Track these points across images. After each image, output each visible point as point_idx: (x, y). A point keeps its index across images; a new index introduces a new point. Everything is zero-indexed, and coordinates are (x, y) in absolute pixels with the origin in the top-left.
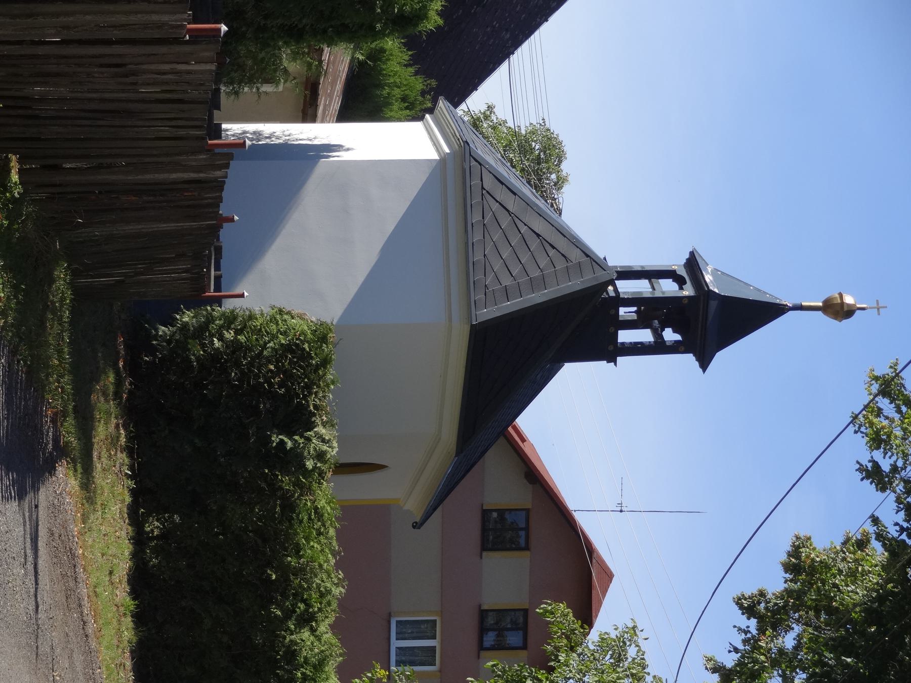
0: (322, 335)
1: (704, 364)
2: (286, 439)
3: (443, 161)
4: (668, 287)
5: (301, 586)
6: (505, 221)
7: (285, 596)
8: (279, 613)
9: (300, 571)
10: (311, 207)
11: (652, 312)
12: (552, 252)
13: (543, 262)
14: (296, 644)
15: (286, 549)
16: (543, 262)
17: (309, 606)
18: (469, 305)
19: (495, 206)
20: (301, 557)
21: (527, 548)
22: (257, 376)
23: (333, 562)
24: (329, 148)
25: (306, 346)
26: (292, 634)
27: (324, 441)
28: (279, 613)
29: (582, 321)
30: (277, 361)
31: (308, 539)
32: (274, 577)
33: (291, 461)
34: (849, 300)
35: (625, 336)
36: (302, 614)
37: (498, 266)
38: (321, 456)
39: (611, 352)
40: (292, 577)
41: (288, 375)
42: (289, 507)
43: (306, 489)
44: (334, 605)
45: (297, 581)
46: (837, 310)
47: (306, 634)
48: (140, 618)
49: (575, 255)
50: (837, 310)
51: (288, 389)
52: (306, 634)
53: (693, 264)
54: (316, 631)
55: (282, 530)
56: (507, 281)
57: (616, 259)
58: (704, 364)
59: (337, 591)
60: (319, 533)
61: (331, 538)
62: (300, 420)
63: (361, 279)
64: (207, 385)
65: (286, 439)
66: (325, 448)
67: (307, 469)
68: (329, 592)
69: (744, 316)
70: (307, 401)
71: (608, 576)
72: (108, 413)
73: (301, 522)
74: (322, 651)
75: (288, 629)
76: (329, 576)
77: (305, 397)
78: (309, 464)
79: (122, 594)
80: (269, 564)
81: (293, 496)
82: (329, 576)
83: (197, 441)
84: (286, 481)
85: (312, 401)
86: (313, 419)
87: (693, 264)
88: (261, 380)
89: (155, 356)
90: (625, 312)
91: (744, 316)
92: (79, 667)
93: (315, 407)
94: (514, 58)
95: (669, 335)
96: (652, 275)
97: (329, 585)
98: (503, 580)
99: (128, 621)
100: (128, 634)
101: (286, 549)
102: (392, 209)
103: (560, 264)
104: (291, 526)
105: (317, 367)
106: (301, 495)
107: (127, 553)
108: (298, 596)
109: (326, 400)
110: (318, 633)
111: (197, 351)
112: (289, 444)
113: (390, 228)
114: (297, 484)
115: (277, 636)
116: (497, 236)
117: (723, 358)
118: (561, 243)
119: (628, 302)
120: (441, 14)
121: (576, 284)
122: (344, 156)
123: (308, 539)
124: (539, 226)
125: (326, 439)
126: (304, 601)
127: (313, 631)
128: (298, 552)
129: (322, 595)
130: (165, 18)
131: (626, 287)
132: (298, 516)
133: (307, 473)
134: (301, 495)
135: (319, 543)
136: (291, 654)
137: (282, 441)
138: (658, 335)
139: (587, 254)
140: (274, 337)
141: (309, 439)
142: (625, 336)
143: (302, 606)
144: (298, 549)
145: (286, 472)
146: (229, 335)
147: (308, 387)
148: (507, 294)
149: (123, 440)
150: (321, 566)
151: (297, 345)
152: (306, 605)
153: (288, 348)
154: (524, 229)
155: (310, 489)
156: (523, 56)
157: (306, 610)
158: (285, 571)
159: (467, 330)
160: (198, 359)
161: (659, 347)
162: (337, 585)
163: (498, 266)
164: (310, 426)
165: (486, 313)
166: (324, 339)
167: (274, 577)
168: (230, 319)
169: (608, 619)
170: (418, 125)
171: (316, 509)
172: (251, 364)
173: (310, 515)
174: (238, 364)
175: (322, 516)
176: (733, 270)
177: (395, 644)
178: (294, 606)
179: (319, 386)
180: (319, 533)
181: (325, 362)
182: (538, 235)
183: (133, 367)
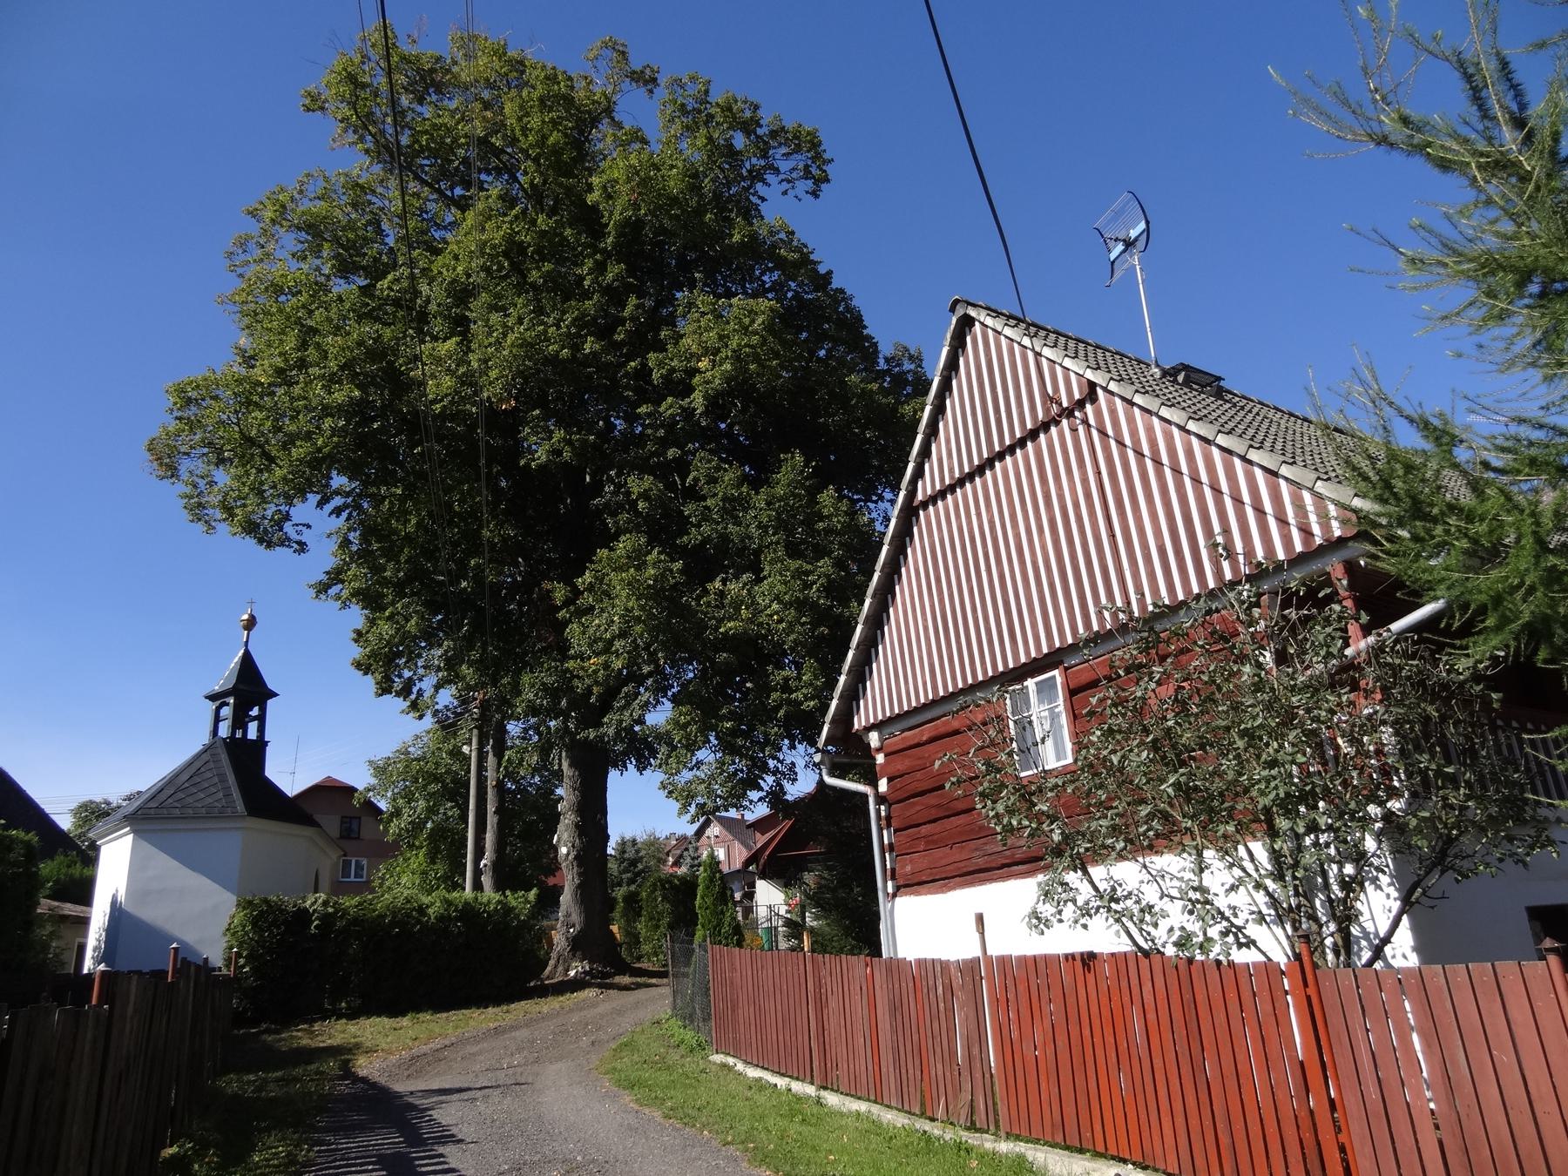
0: (245, 904)
3: (134, 831)
4: (226, 712)
9: (394, 914)
10: (151, 914)
11: (240, 721)
13: (209, 775)
16: (209, 775)
18: (235, 817)
24: (114, 903)
29: (245, 756)
33: (327, 920)
34: (246, 617)
37: (210, 800)
38: (325, 904)
42: (356, 921)
43: (345, 912)
46: (251, 624)
47: (431, 911)
48: (418, 1009)
49: (206, 757)
50: (251, 624)
52: (431, 911)
53: (212, 697)
56: (221, 795)
57: (204, 738)
62: (303, 915)
69: (248, 668)
72: (292, 1037)
79: (405, 1021)
85: (290, 908)
87: (212, 697)
90: (239, 734)
91: (248, 668)
92: (475, 1049)
94: (47, 811)
95: (255, 712)
96: (217, 719)
99: (421, 1015)
100: (427, 1016)
102: (164, 864)
103: (212, 765)
108: (408, 915)
109: (289, 901)
114: (342, 917)
116: (190, 800)
118: (198, 764)
119: (233, 733)
120: (27, 832)
121: (224, 757)
122: (122, 896)
124: (185, 777)
125: (314, 901)
130: (89, 1036)
131: (224, 731)
138: (255, 718)
139: (204, 751)
140: (247, 934)
142: (252, 733)
147: (281, 911)
148: (228, 795)
153: (254, 924)
156: (48, 808)
158: (393, 924)
161: (261, 719)
163: (210, 800)
164: (306, 910)
165: (240, 807)
166: (250, 903)
168: (228, 961)
169: (359, 778)
170: (103, 849)
172: (263, 947)
176: (224, 674)
177: (352, 879)
181: (266, 901)
183: (256, 1023)
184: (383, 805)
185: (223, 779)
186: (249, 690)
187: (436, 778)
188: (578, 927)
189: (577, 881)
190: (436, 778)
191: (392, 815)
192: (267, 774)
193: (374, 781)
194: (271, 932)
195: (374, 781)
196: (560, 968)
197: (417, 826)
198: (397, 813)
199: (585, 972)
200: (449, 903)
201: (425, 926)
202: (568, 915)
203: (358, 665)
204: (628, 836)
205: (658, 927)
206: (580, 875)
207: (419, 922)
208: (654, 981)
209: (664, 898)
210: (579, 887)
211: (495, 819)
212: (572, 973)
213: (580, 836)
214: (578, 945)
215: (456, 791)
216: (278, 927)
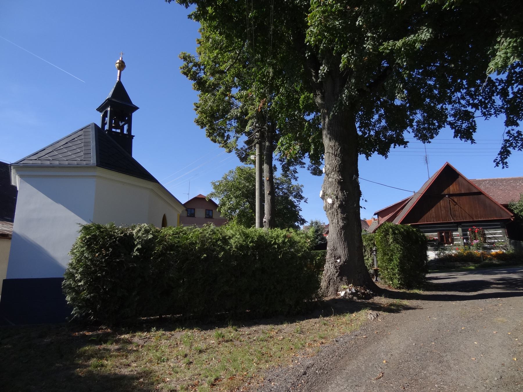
1: (136, 108)
2: (136, 248)
5: (209, 243)
6: (56, 153)
7: (214, 250)
8: (222, 253)
9: (203, 243)
12: (76, 139)
14: (237, 245)
15: (192, 250)
17: (219, 239)
19: (47, 156)
20: (196, 242)
21: (194, 209)
22: (101, 262)
23: (198, 229)
25: (87, 237)
26: (232, 247)
27: (140, 230)
28: (222, 253)
30: (94, 252)
31: (187, 239)
32: (205, 255)
33: (148, 246)
35: (125, 132)
36: (223, 242)
39: (130, 137)
40: (205, 247)
41: (103, 246)
42: (172, 247)
43: (163, 239)
44: (218, 228)
45: (208, 244)
47: (232, 241)
50: (122, 66)
51: (110, 246)
52: (232, 241)
54: (230, 237)
55: (183, 251)
58: (136, 108)
59: (212, 227)
60: (185, 234)
61: (187, 228)
62: (127, 241)
63: (72, 214)
64: (104, 289)
65: (136, 248)
66: (143, 230)
67: (152, 238)
68: (212, 230)
69: (120, 89)
70: (118, 237)
71: (200, 195)
73: (179, 241)
74: (240, 234)
75: (229, 249)
76: (205, 230)
77: (115, 238)
78: (150, 236)
80: (199, 257)
81: (166, 245)
82: (205, 230)
83: (134, 294)
84: (158, 249)
86: (128, 234)
88: (103, 260)
89: (91, 314)
91: (120, 89)
93: (121, 233)
97: (210, 230)
98: (200, 213)
100: (229, 332)
101: (192, 250)
104: (180, 246)
105: (100, 232)
106: (166, 241)
107: (189, 333)
108: (214, 244)
110: (231, 236)
111: (85, 295)
112: (139, 246)
113: (50, 200)
114: (160, 243)
115: (233, 254)
117: (135, 102)
121: (92, 134)
123: (187, 239)
125: (138, 230)
126: (217, 241)
127: (230, 238)
128: (193, 244)
129: (214, 233)
132: (176, 243)
133: (155, 237)
134: (166, 241)
135: (190, 234)
136: (241, 247)
137: (137, 250)
141: (139, 237)
142: (125, 132)
143: (219, 242)
144: (192, 244)
145: (153, 249)
146: (78, 276)
147: (111, 236)
149: (127, 336)
150: (201, 233)
151: (87, 241)
152: (218, 241)
154: (62, 147)
155: (163, 237)
157: (221, 240)
158: (202, 250)
159: (99, 169)
160: (89, 293)
162: (210, 227)
163: (74, 156)
164: (131, 235)
165: (93, 160)
167: (205, 255)
171: (173, 234)
172: (95, 265)
173: (176, 237)
174: (95, 272)
175: (177, 232)
178: (219, 246)
179: (111, 231)
180: (185, 234)
181: (99, 227)
182: (67, 143)
184: (217, 201)
185: (87, 144)
186: (120, 106)
187: (238, 189)
188: (343, 259)
189: (341, 224)
190: (238, 189)
191: (222, 205)
192: (135, 155)
193: (214, 191)
194: (101, 253)
195: (214, 191)
196: (331, 289)
197: (233, 209)
198: (224, 204)
199: (352, 293)
200: (247, 236)
201: (227, 252)
202: (335, 249)
203: (197, 122)
204: (314, 220)
205: (391, 260)
206: (343, 219)
207: (223, 249)
208: (405, 302)
209: (395, 240)
210: (343, 228)
211: (269, 197)
212: (342, 294)
213: (342, 190)
214: (345, 272)
215: (250, 195)
216: (107, 249)
